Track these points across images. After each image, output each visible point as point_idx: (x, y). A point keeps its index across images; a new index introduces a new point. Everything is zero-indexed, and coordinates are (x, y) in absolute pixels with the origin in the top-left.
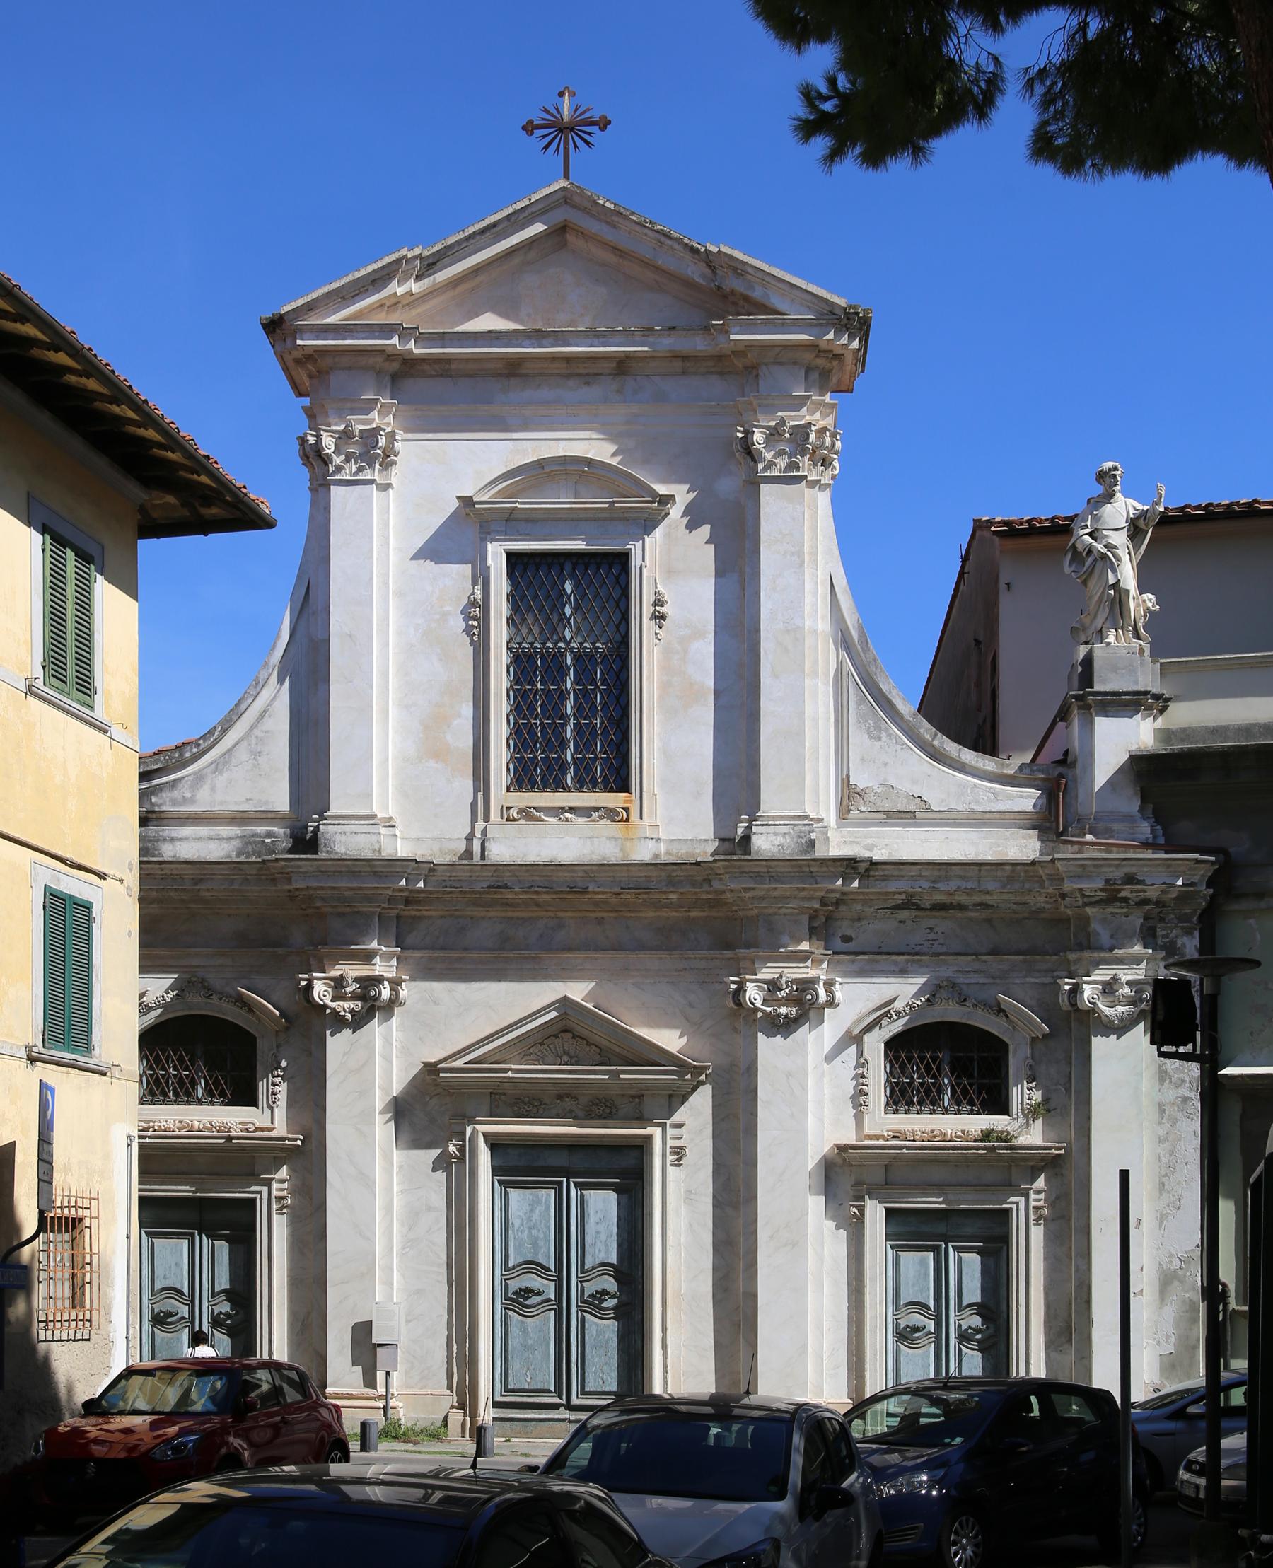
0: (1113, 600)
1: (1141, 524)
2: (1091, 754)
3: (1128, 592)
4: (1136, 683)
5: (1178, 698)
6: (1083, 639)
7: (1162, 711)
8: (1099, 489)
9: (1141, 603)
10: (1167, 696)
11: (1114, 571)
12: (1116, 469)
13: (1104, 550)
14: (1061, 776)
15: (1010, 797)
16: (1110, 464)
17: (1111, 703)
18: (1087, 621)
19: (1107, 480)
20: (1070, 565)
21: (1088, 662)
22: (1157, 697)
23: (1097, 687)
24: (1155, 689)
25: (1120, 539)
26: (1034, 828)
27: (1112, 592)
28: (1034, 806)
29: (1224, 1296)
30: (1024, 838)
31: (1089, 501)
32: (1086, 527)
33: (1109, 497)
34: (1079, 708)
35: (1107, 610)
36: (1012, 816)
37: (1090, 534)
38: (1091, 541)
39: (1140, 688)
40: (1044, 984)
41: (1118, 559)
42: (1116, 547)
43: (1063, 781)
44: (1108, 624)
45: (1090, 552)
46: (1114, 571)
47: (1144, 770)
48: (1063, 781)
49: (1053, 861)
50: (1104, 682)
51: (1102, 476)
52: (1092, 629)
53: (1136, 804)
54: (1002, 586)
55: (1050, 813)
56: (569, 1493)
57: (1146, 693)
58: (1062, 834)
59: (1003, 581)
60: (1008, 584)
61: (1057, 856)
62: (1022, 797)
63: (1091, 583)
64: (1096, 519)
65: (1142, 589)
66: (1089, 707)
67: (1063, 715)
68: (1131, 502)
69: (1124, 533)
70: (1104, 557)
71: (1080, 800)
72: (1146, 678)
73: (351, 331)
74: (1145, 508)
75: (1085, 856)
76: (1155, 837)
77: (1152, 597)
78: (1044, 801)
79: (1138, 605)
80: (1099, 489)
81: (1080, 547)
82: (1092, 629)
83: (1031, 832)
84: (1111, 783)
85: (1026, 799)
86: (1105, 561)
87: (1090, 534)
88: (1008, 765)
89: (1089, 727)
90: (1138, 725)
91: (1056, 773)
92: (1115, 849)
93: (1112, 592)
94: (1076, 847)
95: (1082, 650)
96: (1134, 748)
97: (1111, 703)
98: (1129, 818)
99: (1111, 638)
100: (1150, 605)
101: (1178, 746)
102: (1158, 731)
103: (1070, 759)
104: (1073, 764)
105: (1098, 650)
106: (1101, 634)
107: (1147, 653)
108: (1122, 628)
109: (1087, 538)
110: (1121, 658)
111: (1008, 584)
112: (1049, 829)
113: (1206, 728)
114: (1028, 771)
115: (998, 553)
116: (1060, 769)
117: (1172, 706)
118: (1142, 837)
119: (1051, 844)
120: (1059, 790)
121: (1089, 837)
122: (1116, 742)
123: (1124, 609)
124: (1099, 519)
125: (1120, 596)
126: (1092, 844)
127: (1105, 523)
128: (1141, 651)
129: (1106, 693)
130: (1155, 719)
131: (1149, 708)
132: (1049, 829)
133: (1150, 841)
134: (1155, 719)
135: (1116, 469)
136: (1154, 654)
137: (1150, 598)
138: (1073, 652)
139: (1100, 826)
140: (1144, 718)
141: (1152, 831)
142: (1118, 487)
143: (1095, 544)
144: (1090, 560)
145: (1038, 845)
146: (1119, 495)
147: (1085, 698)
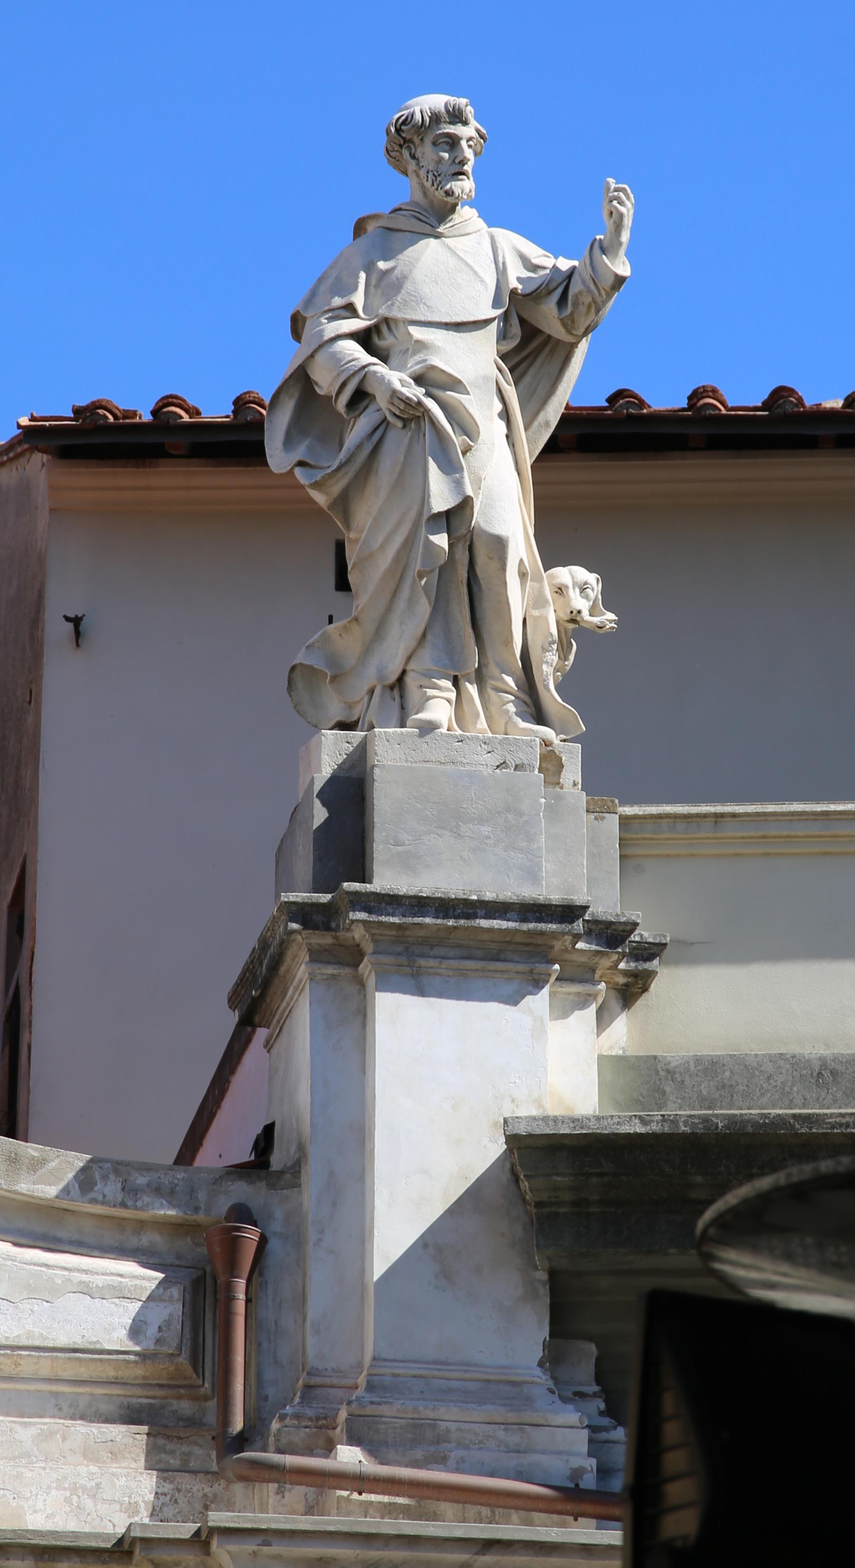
0: (446, 569)
1: (549, 318)
2: (360, 1135)
3: (499, 545)
4: (533, 875)
5: (691, 952)
6: (336, 711)
7: (631, 991)
9: (548, 598)
10: (644, 934)
11: (450, 467)
12: (456, 116)
13: (415, 392)
14: (242, 1214)
15: (43, 1291)
16: (436, 101)
17: (433, 943)
18: (348, 643)
19: (427, 152)
20: (289, 442)
21: (351, 792)
22: (612, 935)
23: (386, 879)
24: (606, 902)
25: (475, 362)
26: (131, 1416)
28: (136, 1331)
30: (89, 1454)
31: (359, 228)
32: (350, 310)
33: (435, 215)
34: (318, 956)
35: (424, 609)
36: (45, 1366)
37: (365, 338)
38: (363, 357)
39: (549, 890)
40: (112, 1395)
41: (467, 428)
42: (455, 384)
43: (251, 1235)
44: (425, 659)
45: (361, 397)
46: (450, 467)
47: (570, 1192)
48: (251, 1235)
49: (201, 1541)
50: (408, 862)
51: (407, 139)
52: (369, 677)
53: (532, 1334)
54: (56, 630)
55: (196, 1361)
57: (569, 912)
58: (242, 1441)
59: (61, 601)
60: (76, 621)
61: (218, 1518)
62: (87, 1291)
64: (387, 285)
65: (554, 546)
66: (352, 956)
67: (255, 1002)
68: (511, 241)
69: (488, 338)
71: (312, 1312)
72: (568, 857)
74: (564, 264)
75: (331, 1522)
76: (603, 1472)
77: (592, 578)
78: (173, 1310)
79: (539, 601)
80: (401, 189)
81: (324, 380)
82: (369, 677)
83: (118, 1432)
84: (433, 1246)
85: (104, 1302)
87: (354, 336)
88: (36, 1165)
89: (352, 1026)
90: (539, 1033)
91: (223, 1205)
92: (447, 1508)
93: (441, 540)
94: (297, 1493)
95: (331, 751)
96: (527, 1110)
97: (433, 943)
98: (506, 1391)
99: (439, 708)
100: (581, 604)
101: (681, 1113)
102: (613, 1067)
103: (277, 1160)
104: (294, 1173)
105: (390, 747)
106: (398, 691)
107: (572, 772)
108: (480, 678)
110: (476, 787)
111: (76, 621)
112: (193, 1423)
113: (796, 1063)
114: (112, 1188)
115: (43, 520)
116: (241, 1191)
117: (667, 981)
118: (559, 1468)
119: (198, 1486)
120: (232, 1268)
121: (349, 1456)
122: (451, 1090)
123: (487, 607)
125: (467, 574)
126: (360, 1482)
127: (420, 300)
128: (551, 763)
129: (419, 904)
130: (603, 1020)
131: (580, 974)
132: (193, 1423)
133: (589, 1482)
134: (603, 1020)
135: (456, 116)
136: (601, 785)
139: (393, 1412)
140: (561, 1011)
141: (596, 1447)
142: (465, 186)
143: (381, 368)
144: (363, 424)
145: (144, 1486)
146: (466, 215)
147: (344, 918)
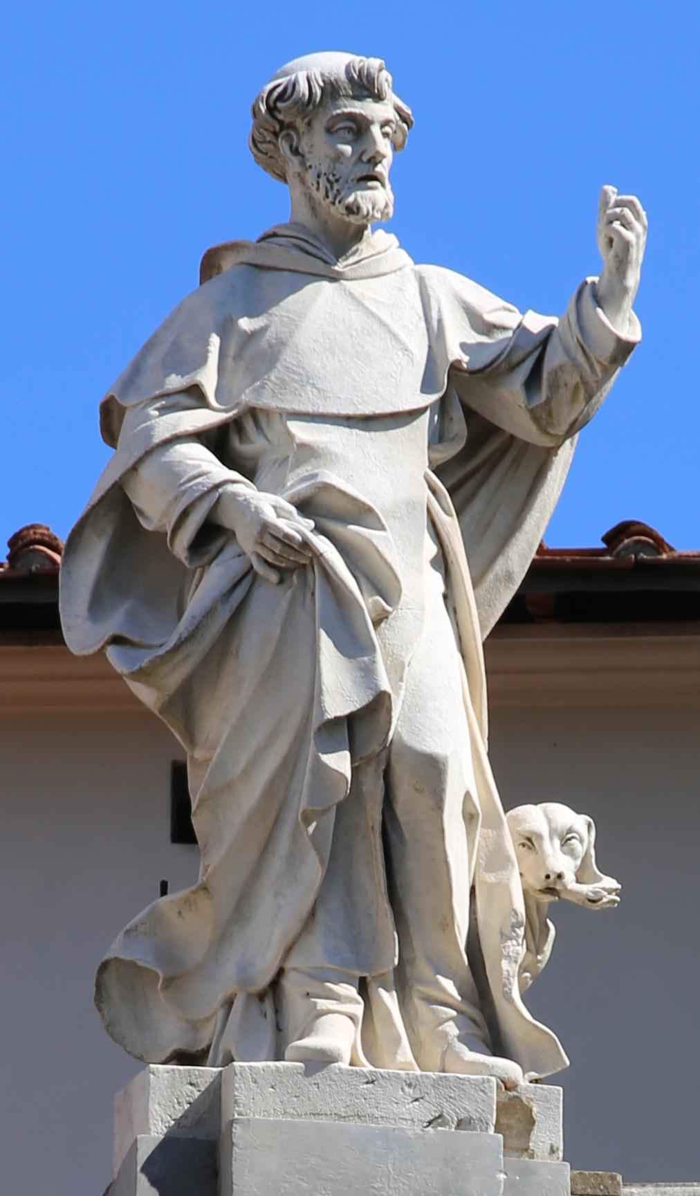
1: (511, 407)
3: (432, 770)
6: (173, 1035)
8: (270, 204)
9: (510, 853)
11: (355, 645)
12: (365, 87)
13: (298, 526)
16: (332, 63)
18: (191, 926)
19: (317, 144)
20: (97, 606)
25: (393, 477)
27: (340, 762)
29: (623, 225)
31: (210, 265)
32: (195, 395)
33: (329, 243)
35: (313, 871)
37: (219, 440)
38: (217, 470)
41: (382, 584)
44: (315, 952)
45: (212, 534)
46: (355, 645)
51: (285, 122)
52: (225, 980)
56: (312, 771)
63: (220, 717)
64: (251, 356)
65: (518, 777)
70: (294, 563)
73: (618, 269)
74: (536, 322)
79: (495, 860)
80: (270, 204)
81: (154, 508)
82: (225, 980)
86: (307, 582)
93: (340, 762)
95: (165, 1097)
99: (336, 1029)
100: (563, 864)
105: (258, 1091)
106: (272, 1007)
107: (549, 1133)
108: (402, 982)
109: (200, 458)
124: (271, 357)
125: (377, 818)
127: (307, 380)
128: (515, 1117)
135: (365, 87)
137: (561, 834)
138: (113, 1095)
143: (243, 488)
146: (380, 244)
